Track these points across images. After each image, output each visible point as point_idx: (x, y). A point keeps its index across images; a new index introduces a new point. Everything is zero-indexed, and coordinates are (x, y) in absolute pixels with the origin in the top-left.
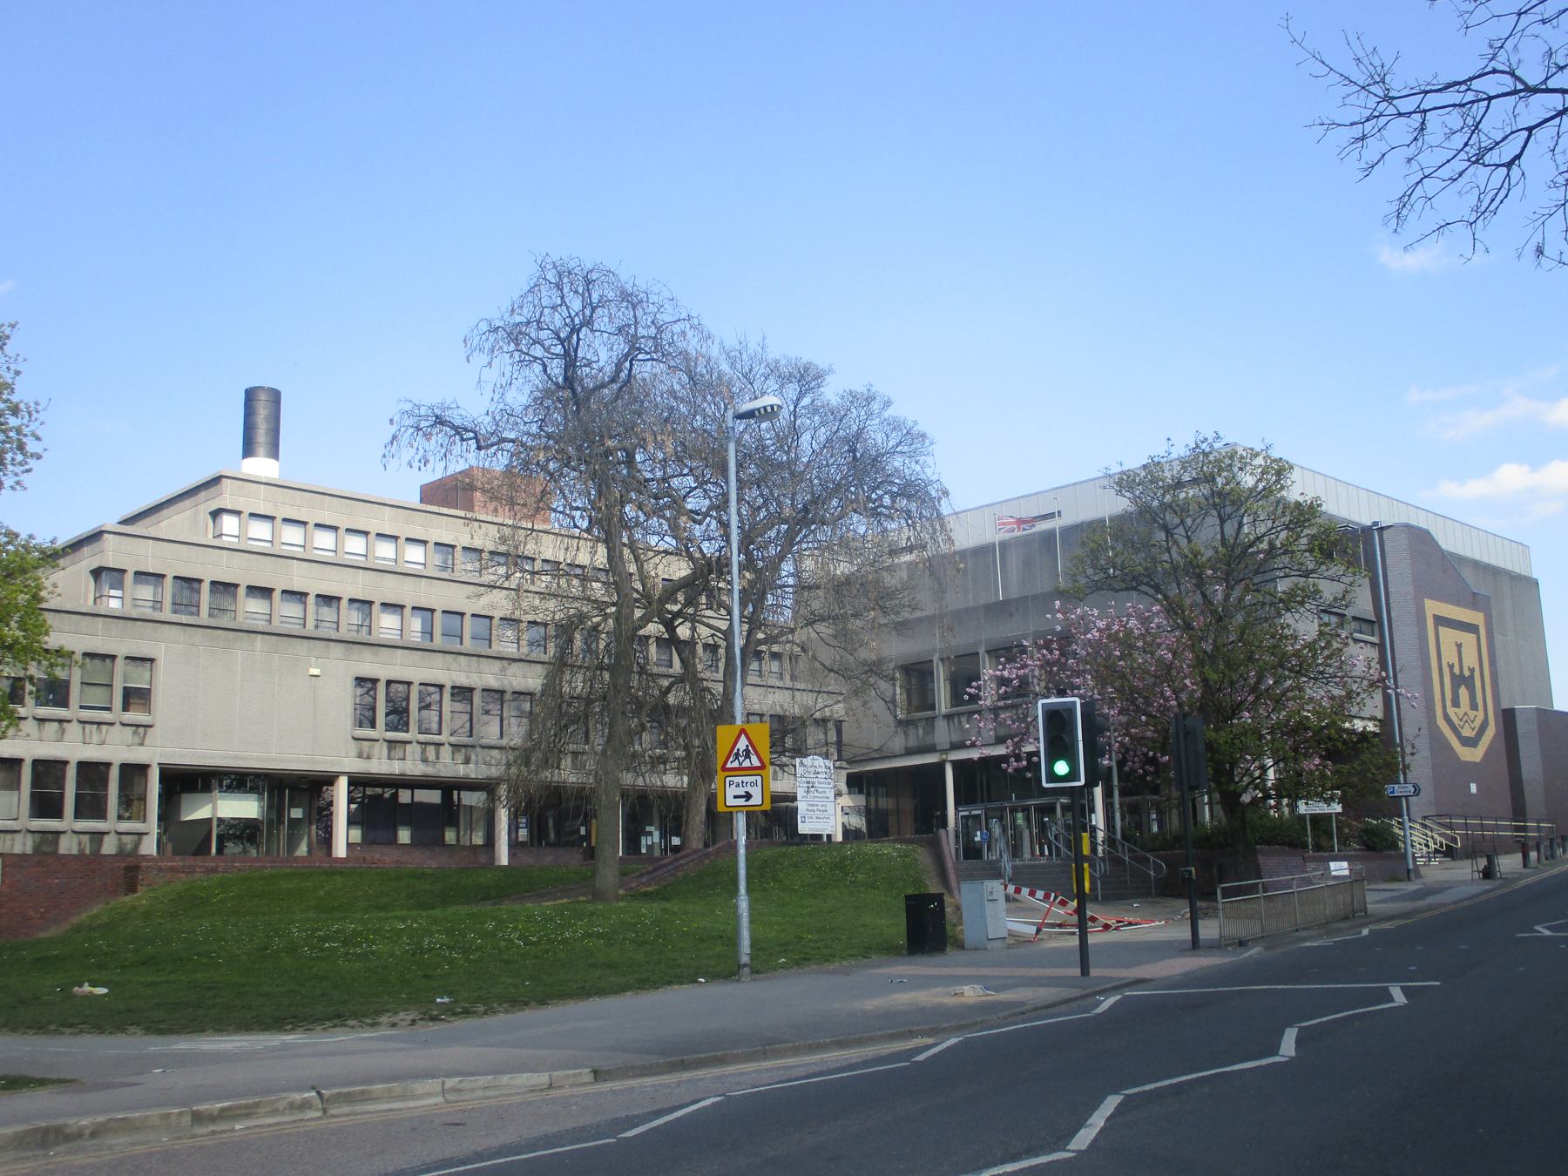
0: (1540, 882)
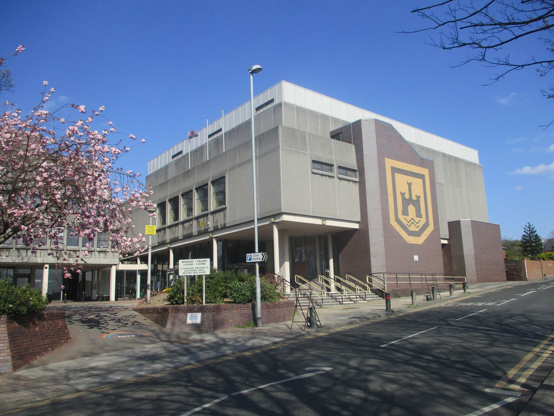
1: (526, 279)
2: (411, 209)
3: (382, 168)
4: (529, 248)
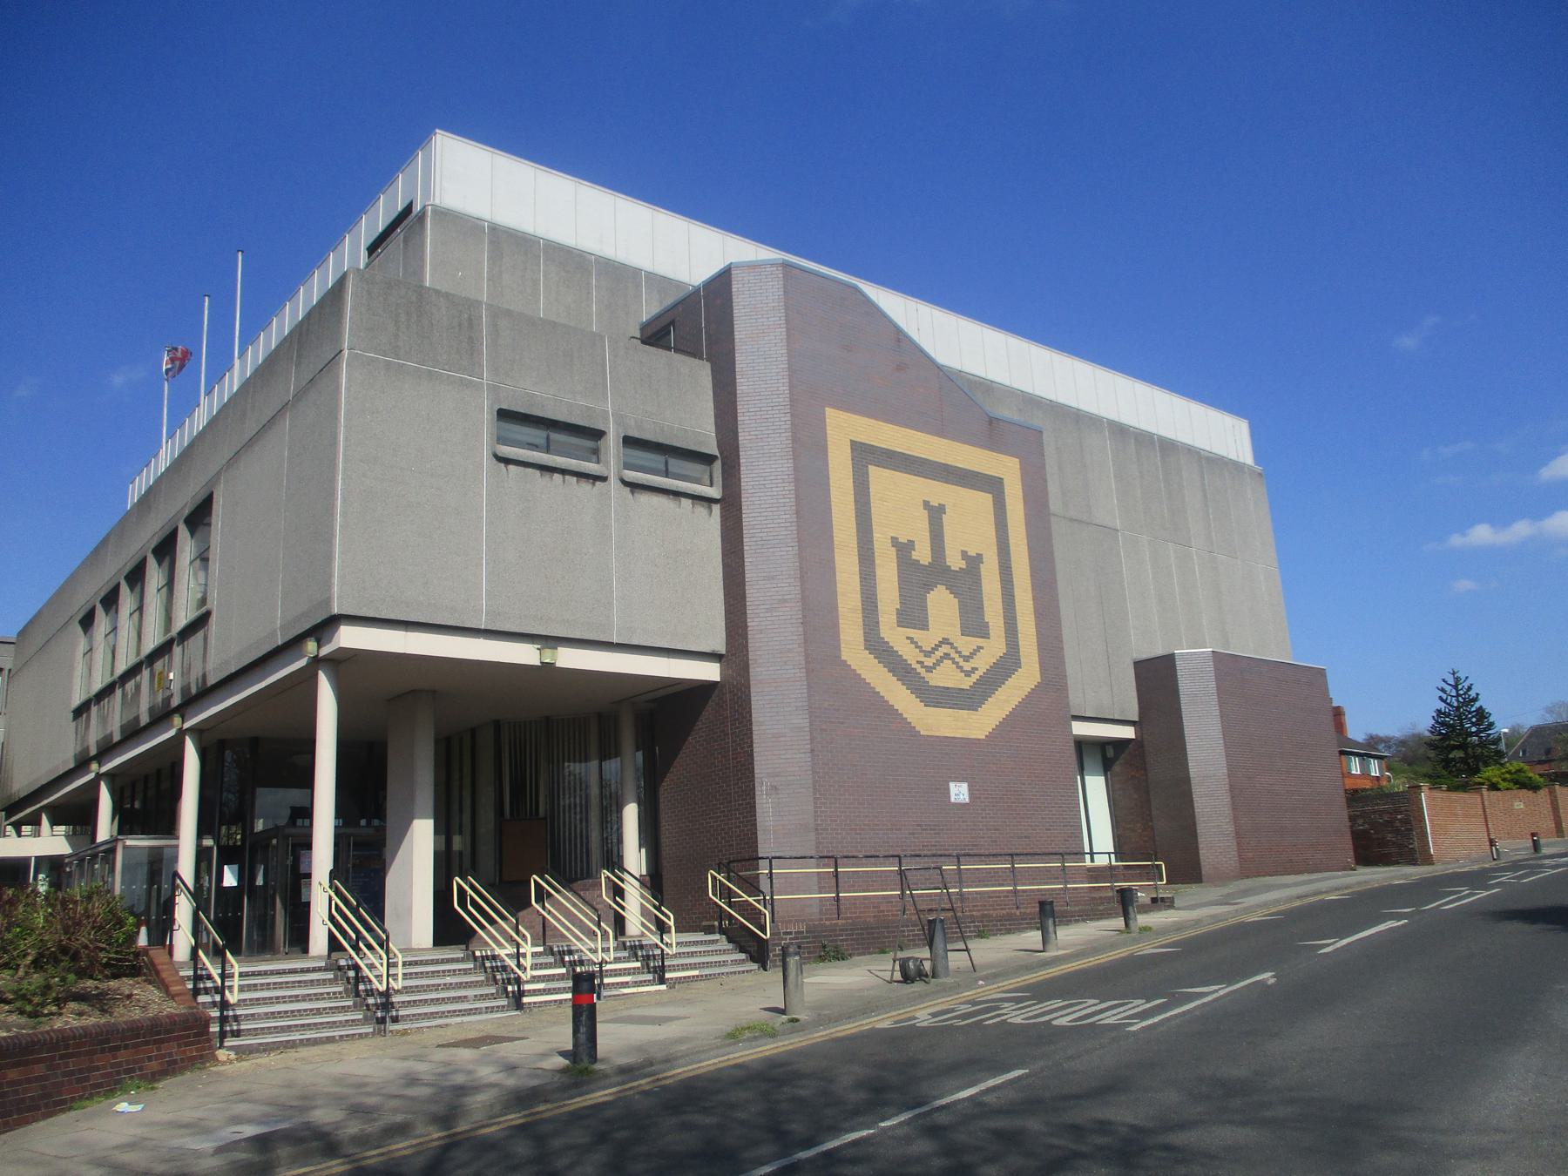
0: (1222, 929)
1: (1428, 860)
2: (942, 604)
3: (808, 447)
4: (1457, 754)
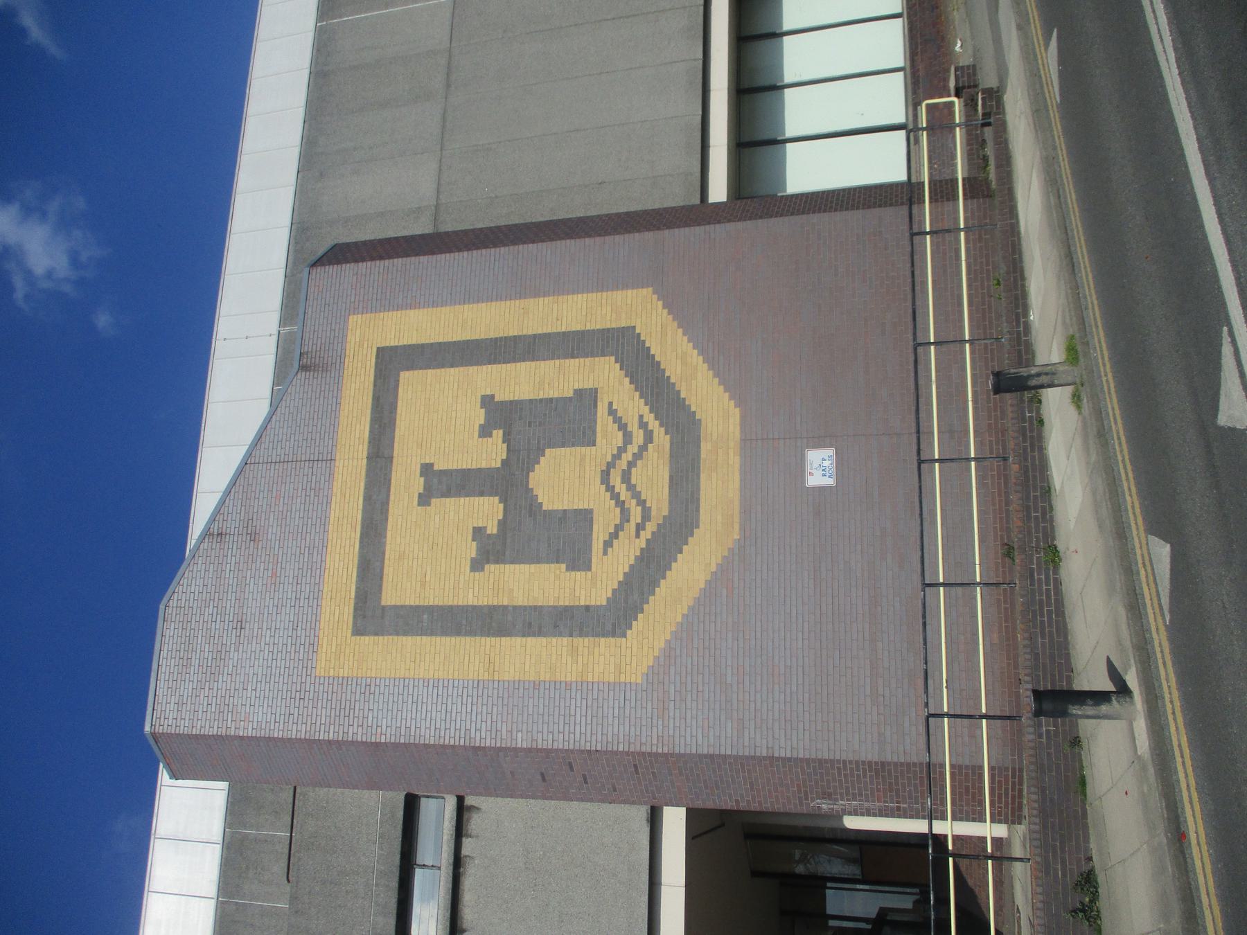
2: (562, 479)
